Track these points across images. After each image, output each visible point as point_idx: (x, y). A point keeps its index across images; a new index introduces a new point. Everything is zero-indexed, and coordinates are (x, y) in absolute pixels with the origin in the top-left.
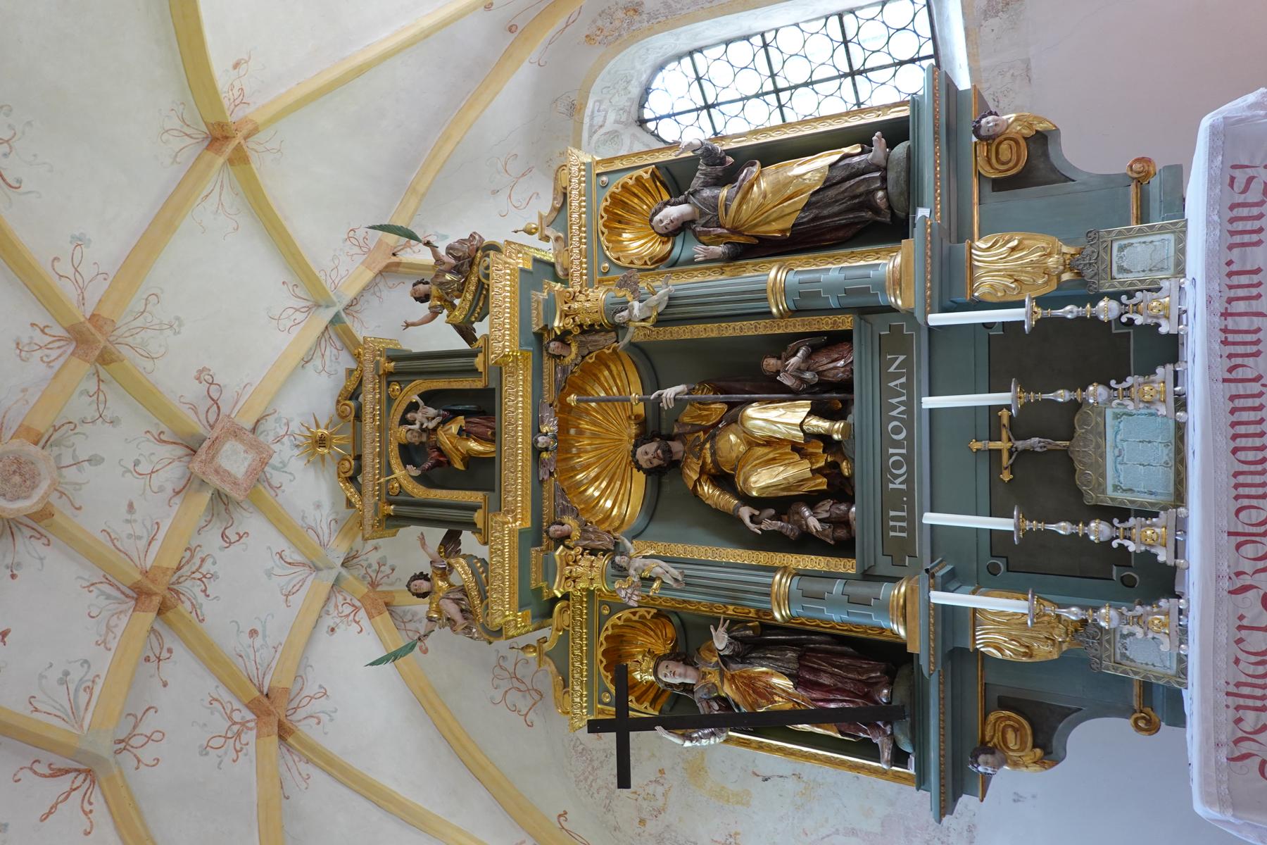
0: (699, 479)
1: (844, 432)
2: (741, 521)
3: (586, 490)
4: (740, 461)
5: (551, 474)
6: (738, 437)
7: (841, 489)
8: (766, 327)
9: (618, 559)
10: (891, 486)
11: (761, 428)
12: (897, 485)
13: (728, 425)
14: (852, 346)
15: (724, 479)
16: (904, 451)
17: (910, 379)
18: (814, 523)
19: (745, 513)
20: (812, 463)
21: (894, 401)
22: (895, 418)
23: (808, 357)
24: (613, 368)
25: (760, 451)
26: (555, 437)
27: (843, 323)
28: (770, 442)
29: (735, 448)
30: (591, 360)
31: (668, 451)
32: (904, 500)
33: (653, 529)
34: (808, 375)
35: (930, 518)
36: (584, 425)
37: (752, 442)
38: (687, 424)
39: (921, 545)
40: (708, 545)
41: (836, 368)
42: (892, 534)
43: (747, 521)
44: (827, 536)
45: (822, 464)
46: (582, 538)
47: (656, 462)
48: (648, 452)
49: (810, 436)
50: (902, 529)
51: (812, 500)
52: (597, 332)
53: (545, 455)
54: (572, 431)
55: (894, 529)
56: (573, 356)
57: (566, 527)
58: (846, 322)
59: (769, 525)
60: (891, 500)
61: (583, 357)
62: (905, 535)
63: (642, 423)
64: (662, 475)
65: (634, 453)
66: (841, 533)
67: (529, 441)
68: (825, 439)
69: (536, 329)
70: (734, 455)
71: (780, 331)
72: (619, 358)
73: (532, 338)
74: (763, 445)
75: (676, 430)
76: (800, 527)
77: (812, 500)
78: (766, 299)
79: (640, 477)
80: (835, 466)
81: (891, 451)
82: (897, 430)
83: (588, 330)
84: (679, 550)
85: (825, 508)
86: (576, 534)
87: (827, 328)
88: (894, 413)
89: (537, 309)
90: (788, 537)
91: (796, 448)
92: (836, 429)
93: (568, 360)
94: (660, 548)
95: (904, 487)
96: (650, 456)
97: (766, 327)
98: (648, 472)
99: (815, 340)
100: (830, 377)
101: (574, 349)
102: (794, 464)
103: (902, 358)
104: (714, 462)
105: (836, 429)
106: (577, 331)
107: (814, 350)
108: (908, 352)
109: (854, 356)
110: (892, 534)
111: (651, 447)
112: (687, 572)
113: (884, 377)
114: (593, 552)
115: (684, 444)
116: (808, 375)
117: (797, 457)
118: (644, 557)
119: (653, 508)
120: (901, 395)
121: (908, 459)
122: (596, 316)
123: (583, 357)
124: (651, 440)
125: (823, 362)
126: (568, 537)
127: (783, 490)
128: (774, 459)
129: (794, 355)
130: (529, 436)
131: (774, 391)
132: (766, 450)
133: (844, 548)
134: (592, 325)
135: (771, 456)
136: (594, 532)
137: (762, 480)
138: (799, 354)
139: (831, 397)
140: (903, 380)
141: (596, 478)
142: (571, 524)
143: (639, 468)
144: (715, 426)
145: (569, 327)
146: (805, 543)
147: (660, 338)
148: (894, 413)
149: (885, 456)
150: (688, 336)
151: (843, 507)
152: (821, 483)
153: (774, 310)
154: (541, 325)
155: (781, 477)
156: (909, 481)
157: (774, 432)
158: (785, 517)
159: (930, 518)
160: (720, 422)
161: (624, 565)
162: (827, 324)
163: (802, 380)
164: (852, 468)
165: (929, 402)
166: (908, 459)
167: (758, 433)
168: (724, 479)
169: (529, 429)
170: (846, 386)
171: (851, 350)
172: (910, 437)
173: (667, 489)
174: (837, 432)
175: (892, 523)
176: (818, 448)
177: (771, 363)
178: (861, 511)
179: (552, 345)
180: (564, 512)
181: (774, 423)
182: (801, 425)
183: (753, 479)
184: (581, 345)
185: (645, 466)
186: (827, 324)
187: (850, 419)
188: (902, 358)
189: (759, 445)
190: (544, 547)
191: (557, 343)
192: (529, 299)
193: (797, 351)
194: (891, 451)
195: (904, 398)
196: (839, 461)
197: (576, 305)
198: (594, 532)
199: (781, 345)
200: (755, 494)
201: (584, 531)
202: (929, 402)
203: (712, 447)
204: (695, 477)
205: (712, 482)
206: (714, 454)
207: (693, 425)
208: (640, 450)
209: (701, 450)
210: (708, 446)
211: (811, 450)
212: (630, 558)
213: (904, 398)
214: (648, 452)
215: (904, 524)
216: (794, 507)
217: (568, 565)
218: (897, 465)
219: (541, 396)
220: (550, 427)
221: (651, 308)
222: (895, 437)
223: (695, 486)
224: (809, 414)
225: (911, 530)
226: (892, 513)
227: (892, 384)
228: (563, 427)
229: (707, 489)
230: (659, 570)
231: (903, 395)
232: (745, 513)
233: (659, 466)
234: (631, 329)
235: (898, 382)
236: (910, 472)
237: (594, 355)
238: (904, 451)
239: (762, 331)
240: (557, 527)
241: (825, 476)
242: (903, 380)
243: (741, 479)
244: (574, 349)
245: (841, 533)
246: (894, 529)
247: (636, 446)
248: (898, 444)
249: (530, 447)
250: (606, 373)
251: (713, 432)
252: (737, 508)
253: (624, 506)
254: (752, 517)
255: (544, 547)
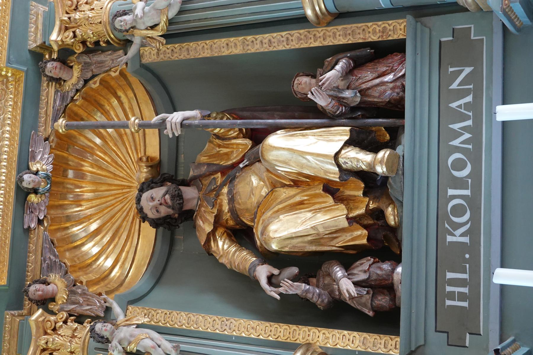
0: (213, 232)
1: (389, 163)
2: (257, 282)
3: (83, 245)
4: (262, 206)
5: (40, 222)
6: (261, 179)
7: (384, 243)
8: (299, 39)
9: (99, 326)
10: (449, 238)
11: (285, 163)
12: (457, 237)
13: (251, 164)
14: (404, 56)
15: (243, 234)
16: (467, 192)
17: (478, 97)
18: (347, 286)
19: (263, 272)
20: (349, 210)
21: (456, 126)
22: (457, 149)
23: (348, 73)
24: (120, 93)
25: (284, 193)
26: (47, 177)
27: (394, 30)
28: (299, 182)
29: (257, 192)
30: (95, 84)
31: (178, 197)
32: (466, 257)
33: (158, 294)
34: (348, 94)
35: (504, 276)
36: (87, 168)
37: (276, 183)
38: (204, 164)
39: (487, 318)
40: (216, 314)
41: (383, 83)
42: (449, 303)
43: (263, 282)
44: (365, 305)
45: (361, 211)
46: (69, 301)
47: (164, 211)
48: (156, 198)
49: (347, 173)
50: (462, 297)
51: (348, 258)
52: (103, 51)
53: (33, 198)
54: (71, 174)
55: (451, 296)
56: (74, 80)
57: (50, 288)
58: (396, 29)
59: (290, 287)
60: (448, 257)
61: (86, 82)
62: (465, 304)
63: (155, 166)
64: (174, 224)
65: (138, 200)
66: (383, 301)
67: (13, 180)
68: (371, 182)
69: (32, 45)
70: (254, 200)
71: (317, 44)
72: (130, 85)
73: (28, 56)
74: (289, 186)
75: (191, 174)
76: (331, 293)
77: (348, 258)
78: (302, 8)
79: (149, 232)
80: (378, 214)
81: (451, 192)
82: (459, 165)
83: (94, 48)
84: (182, 319)
85: (364, 269)
86: (62, 296)
87: (374, 38)
88: (456, 143)
89: (36, 22)
90: (314, 305)
91: (330, 189)
92: (378, 162)
93: (68, 86)
94: (161, 317)
95: (466, 240)
96: (156, 202)
97: (299, 39)
98: (155, 223)
99: (357, 53)
100: (375, 96)
101: (76, 72)
102: (326, 210)
103: (468, 70)
104: (233, 211)
105: (378, 162)
106: (79, 49)
107: (358, 64)
108: (476, 62)
109: (406, 69)
110: (449, 303)
111: (158, 192)
112: (183, 347)
113: (445, 95)
114: (80, 319)
115: (200, 190)
116: (348, 94)
117: (330, 200)
118: (138, 326)
119: (161, 270)
120: (466, 118)
121: (473, 203)
122: (100, 28)
123: (86, 82)
124: (161, 184)
125: (367, 77)
126: (53, 299)
127: (311, 242)
128: (301, 203)
129: (333, 68)
130: (14, 173)
131: (307, 114)
132: (292, 192)
133: (386, 321)
134: (97, 43)
135: (298, 199)
136: (84, 294)
137: (284, 229)
138: (338, 67)
139: (376, 122)
140: (469, 99)
141: (97, 232)
142: (57, 285)
143: (144, 218)
144: (234, 166)
145: (69, 41)
146: (337, 314)
147: (175, 57)
148: (456, 143)
149: (442, 198)
150: (207, 54)
151: (386, 266)
152: (360, 236)
153: (309, 12)
154: (39, 43)
155: (309, 225)
156: (473, 232)
157: (302, 166)
158: (314, 280)
159: (504, 276)
160: (241, 160)
161: (106, 334)
162: (374, 32)
163: (340, 101)
164: (401, 217)
165: (506, 113)
166: (473, 203)
167: (282, 169)
168: (243, 234)
169: (15, 165)
170: (395, 109)
171: (402, 61)
172: (476, 174)
173: (180, 248)
174: (381, 162)
175: (449, 289)
176: (356, 190)
177: (303, 83)
178: (410, 273)
179: (49, 65)
180: (51, 268)
181: (302, 154)
182: (337, 155)
183: (273, 227)
184: (86, 66)
185: (151, 214)
186: (374, 32)
187: (399, 150)
188: (468, 70)
189: (284, 186)
190: (25, 312)
191: (55, 64)
192: (27, 12)
193: (336, 64)
194: (451, 192)
195: (469, 123)
196: (382, 206)
197: (77, 15)
198: (84, 294)
199: (315, 61)
200: (274, 247)
201: (72, 292)
202: (506, 113)
203: (230, 192)
204: (208, 228)
205: (229, 236)
206: (232, 200)
207: (209, 165)
208: (146, 195)
209: (218, 196)
210: (225, 190)
211: (348, 193)
212: (116, 326)
213: (469, 123)
214: (156, 198)
215: (465, 290)
216: (324, 267)
217: (46, 333)
218: (458, 211)
219: (35, 127)
220: (42, 164)
221: (160, 11)
222: (456, 174)
223: (208, 241)
224: (347, 144)
225: (473, 298)
226: (450, 275)
227: (454, 105)
228: (60, 166)
229: (223, 246)
230: (148, 343)
231: (467, 118)
232: (263, 272)
233: (168, 217)
234: (137, 41)
235: (462, 102)
236: (475, 220)
237: (98, 79)
238: (467, 192)
239: (295, 45)
240: (38, 286)
241: (365, 227)
242: (469, 99)
243: (260, 228)
244: (76, 72)
245: (383, 301)
246: (451, 296)
247: (142, 190)
248: (459, 183)
249: (13, 187)
250: (115, 102)
251: (231, 172)
252: (253, 267)
253: (127, 266)
254: (270, 279)
255: (25, 312)
